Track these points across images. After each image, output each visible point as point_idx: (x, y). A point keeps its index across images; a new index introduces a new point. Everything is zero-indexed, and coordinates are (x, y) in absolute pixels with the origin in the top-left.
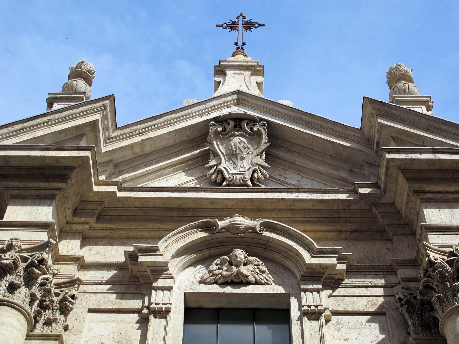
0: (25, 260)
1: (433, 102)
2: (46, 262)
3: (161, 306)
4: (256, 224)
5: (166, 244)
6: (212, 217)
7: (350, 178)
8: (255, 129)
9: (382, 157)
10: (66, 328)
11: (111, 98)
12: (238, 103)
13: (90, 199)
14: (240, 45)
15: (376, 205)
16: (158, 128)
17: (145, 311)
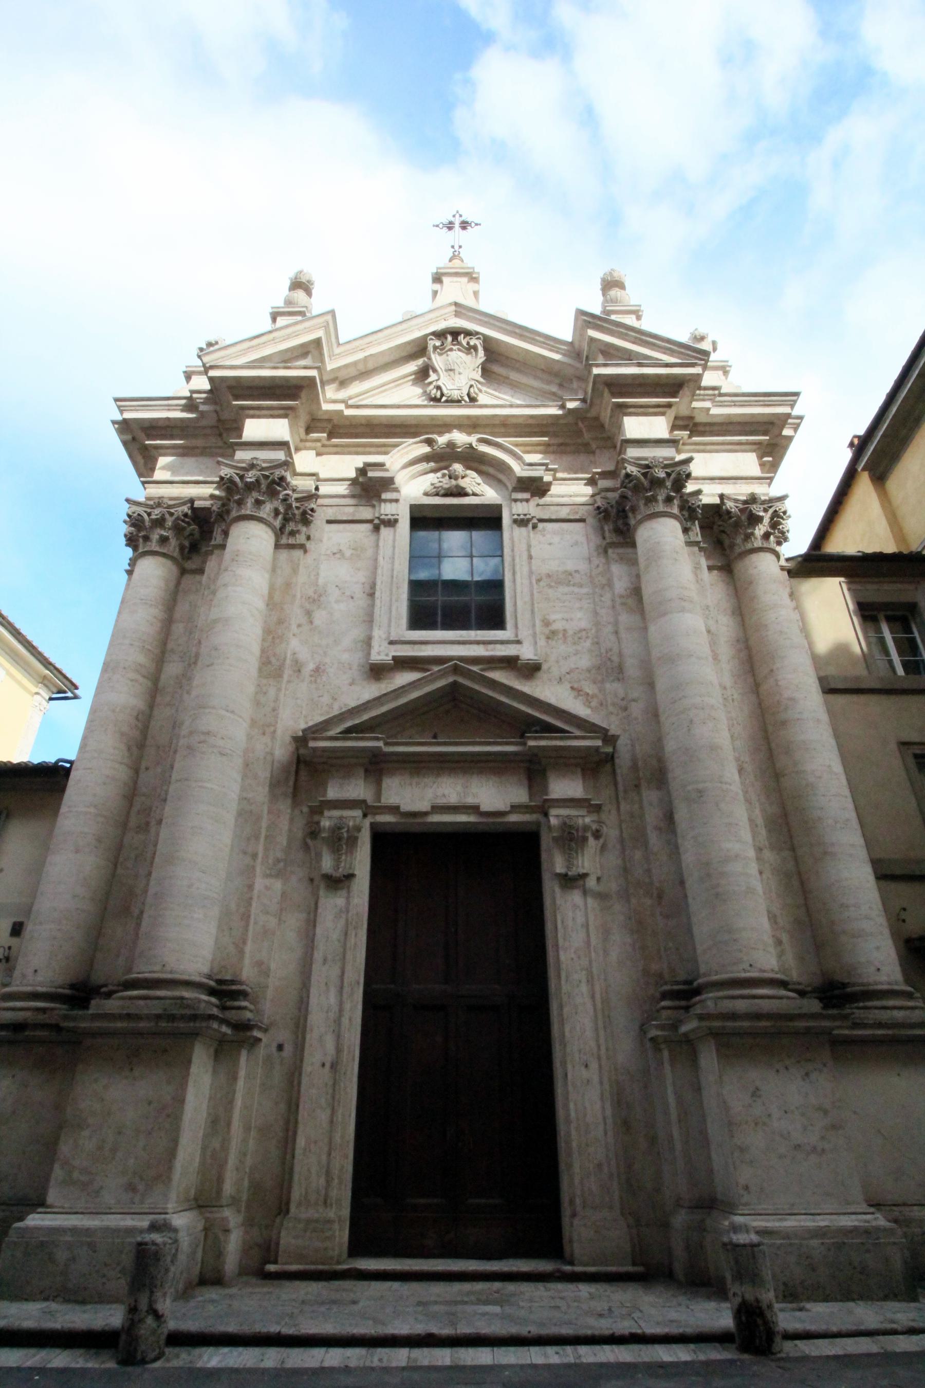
0: (266, 477)
1: (642, 311)
2: (286, 479)
3: (389, 517)
4: (473, 439)
5: (392, 460)
6: (432, 433)
7: (560, 392)
8: (472, 343)
9: (590, 372)
10: (308, 538)
11: (332, 313)
12: (457, 314)
13: (319, 418)
14: (456, 248)
15: (583, 419)
16: (379, 344)
17: (376, 521)
